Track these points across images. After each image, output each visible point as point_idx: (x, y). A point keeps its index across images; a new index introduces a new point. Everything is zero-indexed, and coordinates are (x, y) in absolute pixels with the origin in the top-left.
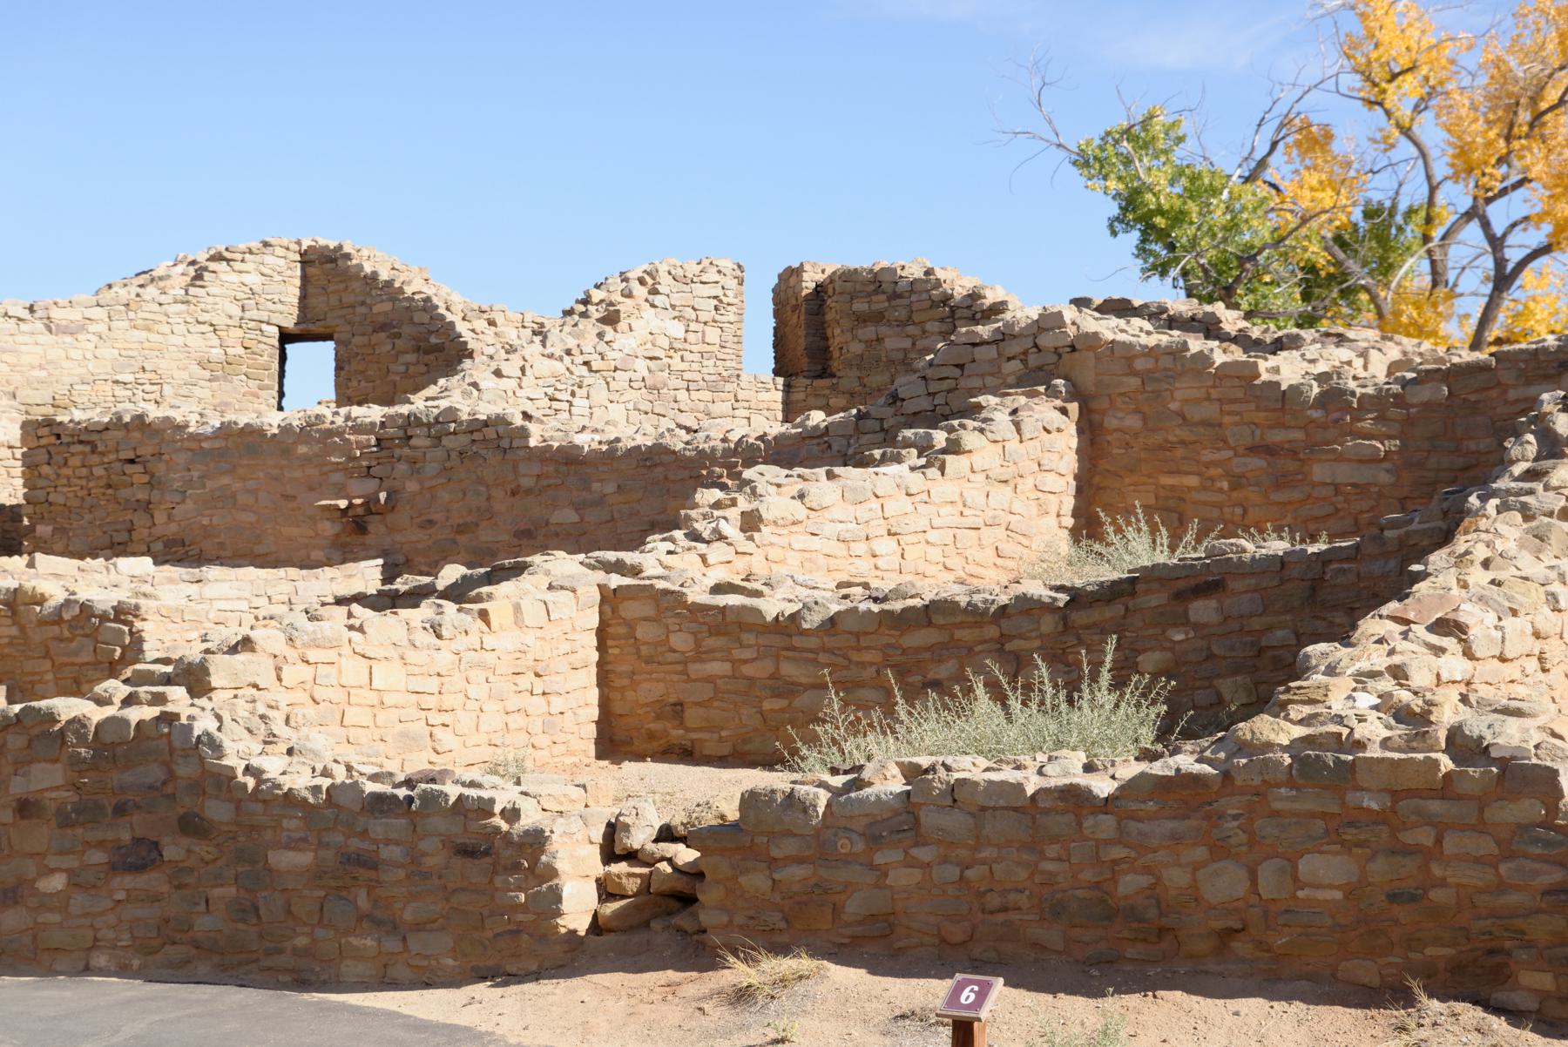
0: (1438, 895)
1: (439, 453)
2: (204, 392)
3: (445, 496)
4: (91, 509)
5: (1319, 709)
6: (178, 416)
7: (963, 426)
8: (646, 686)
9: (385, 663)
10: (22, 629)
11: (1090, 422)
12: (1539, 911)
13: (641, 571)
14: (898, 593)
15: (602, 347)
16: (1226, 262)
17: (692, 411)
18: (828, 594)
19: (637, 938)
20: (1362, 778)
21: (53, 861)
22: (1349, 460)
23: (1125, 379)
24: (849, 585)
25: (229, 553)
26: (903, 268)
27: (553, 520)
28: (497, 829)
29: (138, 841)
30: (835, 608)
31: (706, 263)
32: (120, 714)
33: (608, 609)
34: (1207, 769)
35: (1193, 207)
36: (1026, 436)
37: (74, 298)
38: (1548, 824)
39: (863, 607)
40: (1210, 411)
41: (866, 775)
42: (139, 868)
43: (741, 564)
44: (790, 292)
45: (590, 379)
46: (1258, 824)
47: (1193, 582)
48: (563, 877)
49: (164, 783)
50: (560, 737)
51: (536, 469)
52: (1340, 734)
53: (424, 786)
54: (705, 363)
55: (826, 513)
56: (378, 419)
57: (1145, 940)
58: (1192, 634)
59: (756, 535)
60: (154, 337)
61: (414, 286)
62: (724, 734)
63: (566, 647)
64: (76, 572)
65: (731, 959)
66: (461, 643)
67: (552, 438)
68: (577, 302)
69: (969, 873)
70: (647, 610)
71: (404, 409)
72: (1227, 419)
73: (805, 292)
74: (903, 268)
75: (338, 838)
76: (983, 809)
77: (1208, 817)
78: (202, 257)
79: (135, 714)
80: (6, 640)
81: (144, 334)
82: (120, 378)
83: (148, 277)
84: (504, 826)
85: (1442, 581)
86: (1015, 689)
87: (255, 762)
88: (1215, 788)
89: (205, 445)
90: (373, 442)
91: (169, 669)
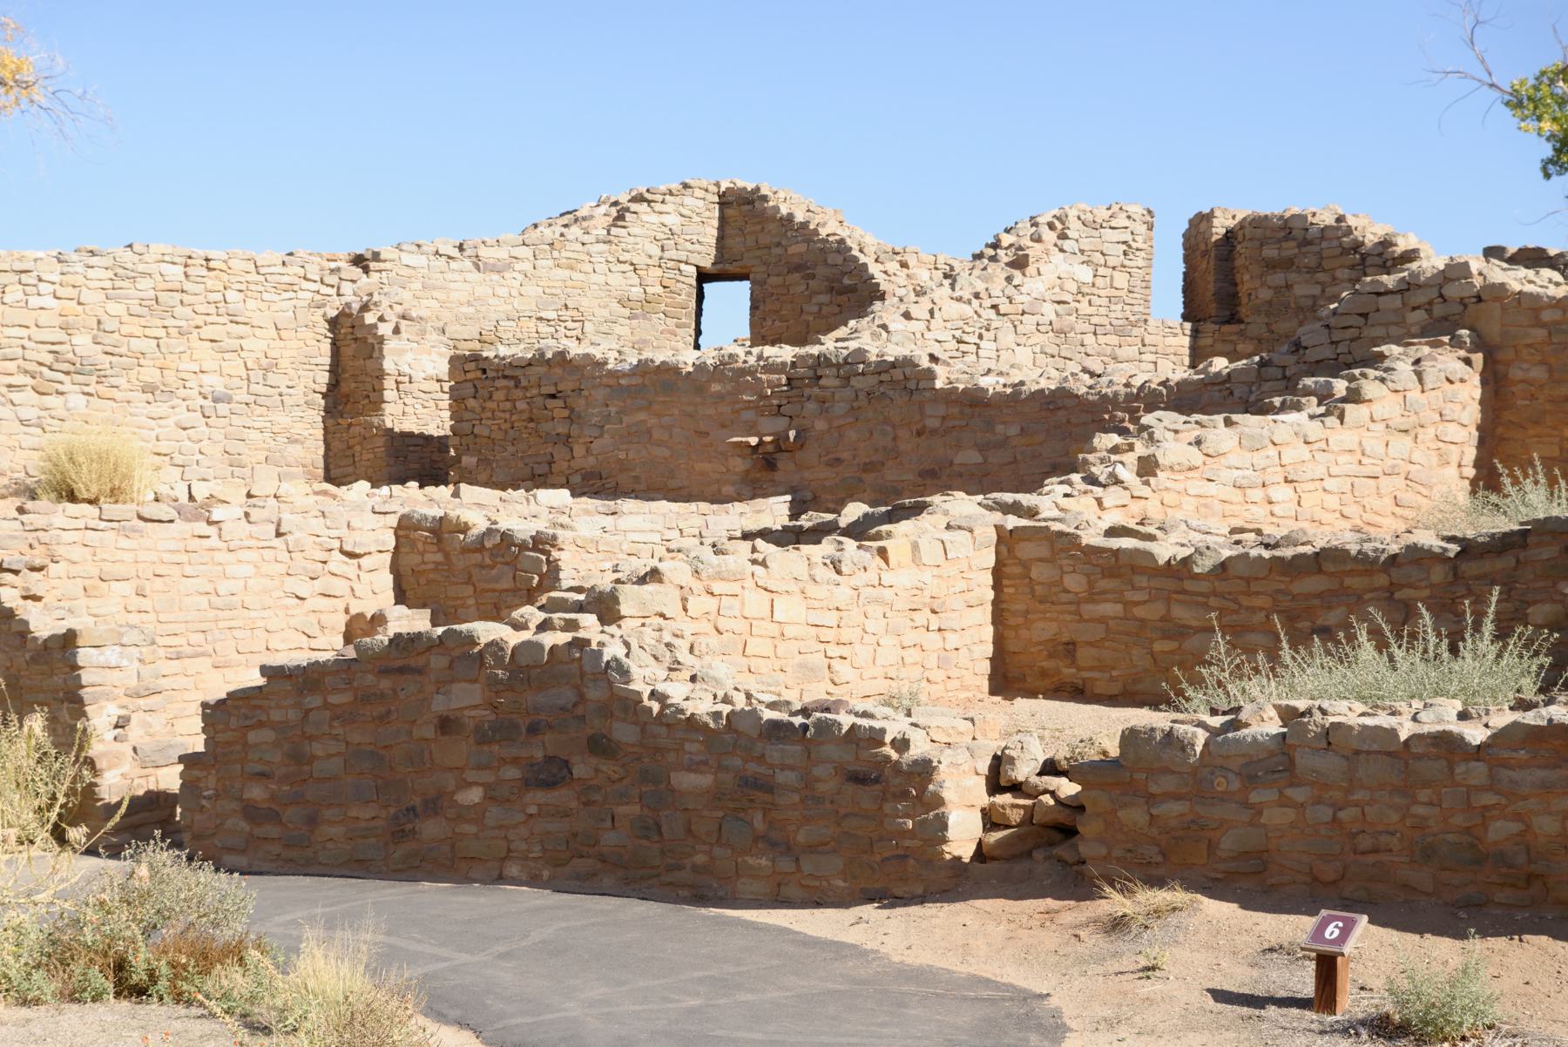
3: (852, 435)
7: (1364, 375)
8: (1040, 625)
10: (447, 555)
11: (1495, 373)
13: (1037, 513)
14: (1289, 540)
15: (1010, 291)
17: (1099, 354)
19: (1020, 867)
21: (470, 776)
24: (1242, 531)
26: (1314, 214)
27: (957, 461)
28: (887, 758)
29: (549, 759)
30: (1226, 553)
31: (1115, 208)
33: (1004, 549)
36: (1428, 385)
39: (1254, 553)
41: (1243, 716)
42: (550, 784)
43: (1136, 508)
45: (997, 322)
48: (950, 806)
49: (575, 705)
50: (954, 673)
51: (941, 410)
53: (818, 715)
54: (1113, 307)
55: (1223, 460)
56: (789, 359)
59: (1152, 480)
60: (576, 276)
61: (829, 228)
63: (962, 585)
65: (1108, 889)
66: (860, 579)
67: (957, 380)
68: (987, 246)
69: (1342, 815)
70: (1043, 551)
71: (814, 350)
73: (1214, 238)
74: (1314, 214)
75: (738, 762)
76: (1357, 753)
78: (624, 199)
79: (550, 639)
80: (432, 566)
81: (567, 273)
82: (543, 314)
83: (572, 217)
84: (894, 756)
87: (661, 687)
89: (623, 382)
90: (784, 381)
91: (582, 597)
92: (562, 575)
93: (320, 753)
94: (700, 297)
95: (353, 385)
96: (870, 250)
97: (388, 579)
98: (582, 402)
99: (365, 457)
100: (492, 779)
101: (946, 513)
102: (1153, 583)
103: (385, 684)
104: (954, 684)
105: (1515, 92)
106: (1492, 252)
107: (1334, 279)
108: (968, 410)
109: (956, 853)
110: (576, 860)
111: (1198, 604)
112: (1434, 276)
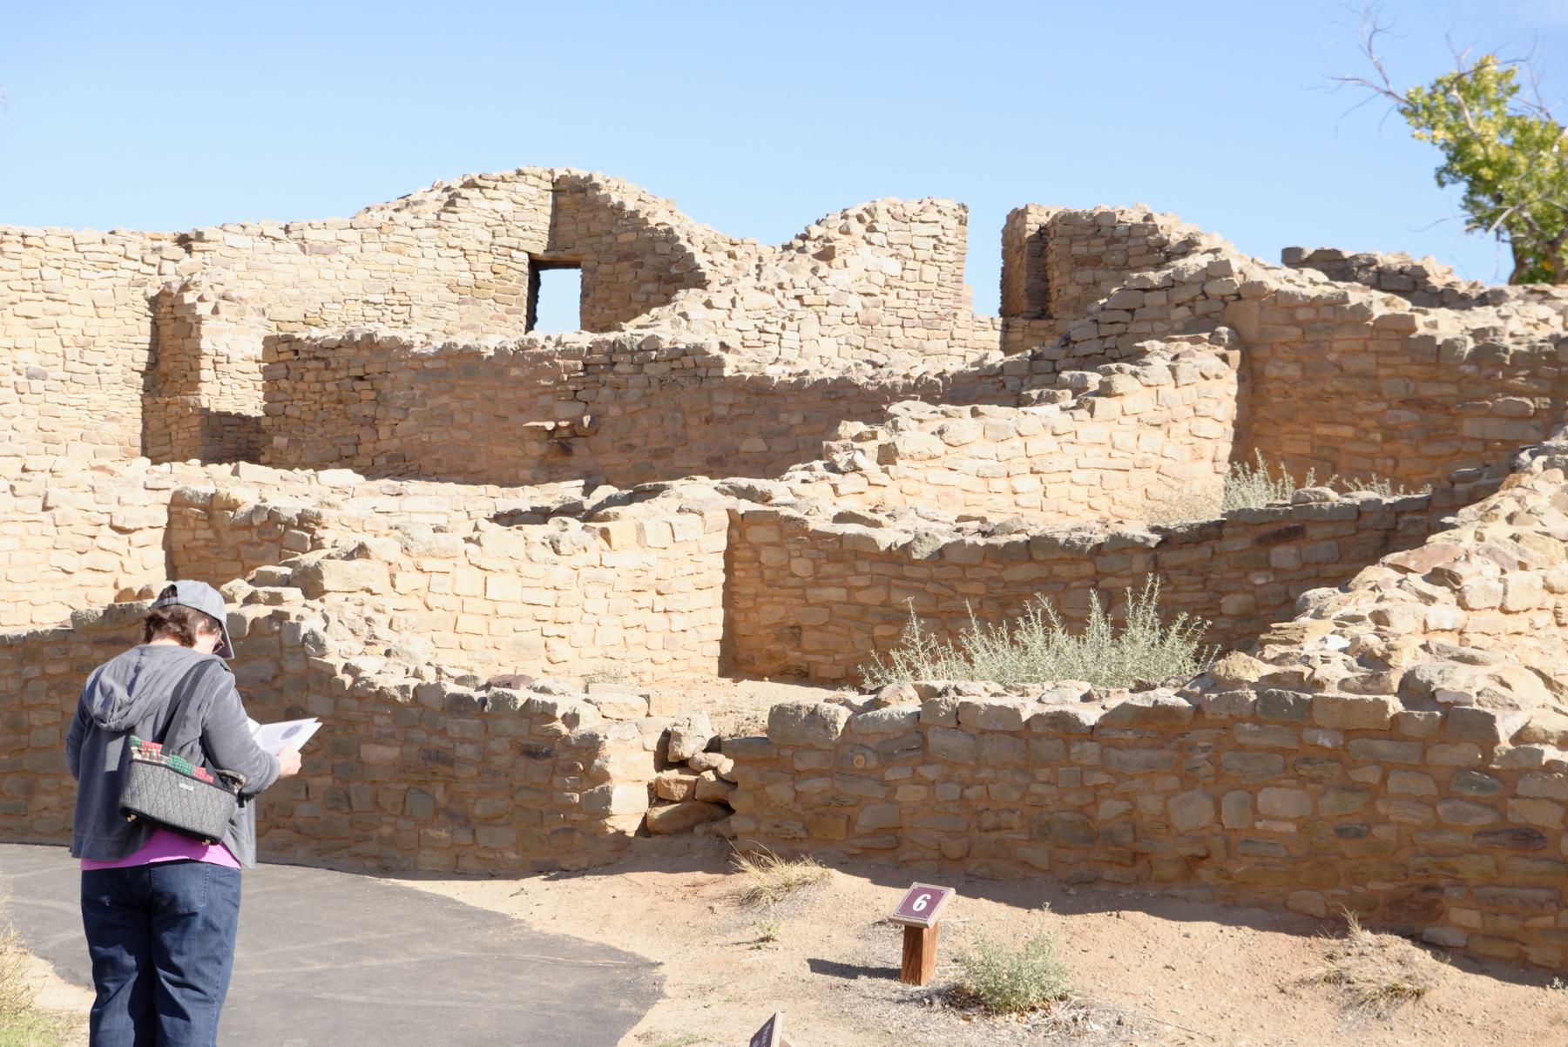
0: (1380, 832)
1: (641, 379)
2: (451, 314)
3: (644, 421)
5: (1294, 649)
7: (1120, 370)
8: (768, 608)
10: (217, 532)
11: (1252, 370)
12: (1473, 852)
14: (1004, 529)
15: (815, 282)
16: (1552, 217)
17: (906, 347)
18: (944, 527)
19: (680, 842)
20: (1318, 716)
22: (1499, 416)
23: (1287, 329)
24: (968, 519)
25: (444, 470)
26: (1122, 212)
27: (743, 448)
28: (558, 732)
30: (945, 540)
31: (927, 202)
33: (735, 533)
34: (1183, 702)
35: (1521, 160)
36: (1182, 381)
38: (1483, 768)
39: (969, 540)
40: (1365, 363)
41: (883, 696)
43: (873, 495)
45: (800, 312)
46: (1225, 756)
47: (1275, 528)
48: (614, 781)
49: (274, 677)
50: (680, 654)
51: (729, 398)
52: (1302, 674)
53: (496, 689)
54: (921, 301)
55: (965, 450)
57: (1119, 863)
58: (1272, 578)
59: (891, 468)
60: (404, 260)
61: (658, 217)
62: (838, 657)
63: (692, 568)
64: (278, 481)
65: (745, 863)
66: (580, 559)
67: (746, 369)
69: (968, 792)
70: (771, 535)
71: (611, 336)
72: (1383, 372)
74: (1122, 212)
75: (423, 735)
76: (983, 732)
77: (1180, 748)
78: (456, 184)
81: (395, 257)
83: (408, 203)
84: (564, 730)
85: (1464, 537)
86: (1035, 614)
87: (354, 661)
88: (1187, 721)
89: (427, 365)
90: (580, 367)
93: (37, 723)
94: (534, 284)
95: (172, 365)
96: (697, 240)
97: (161, 555)
98: (388, 384)
99: (182, 436)
101: (680, 496)
104: (676, 666)
105: (1410, 101)
106: (1292, 257)
108: (754, 399)
109: (620, 828)
110: (273, 831)
112: (1197, 273)
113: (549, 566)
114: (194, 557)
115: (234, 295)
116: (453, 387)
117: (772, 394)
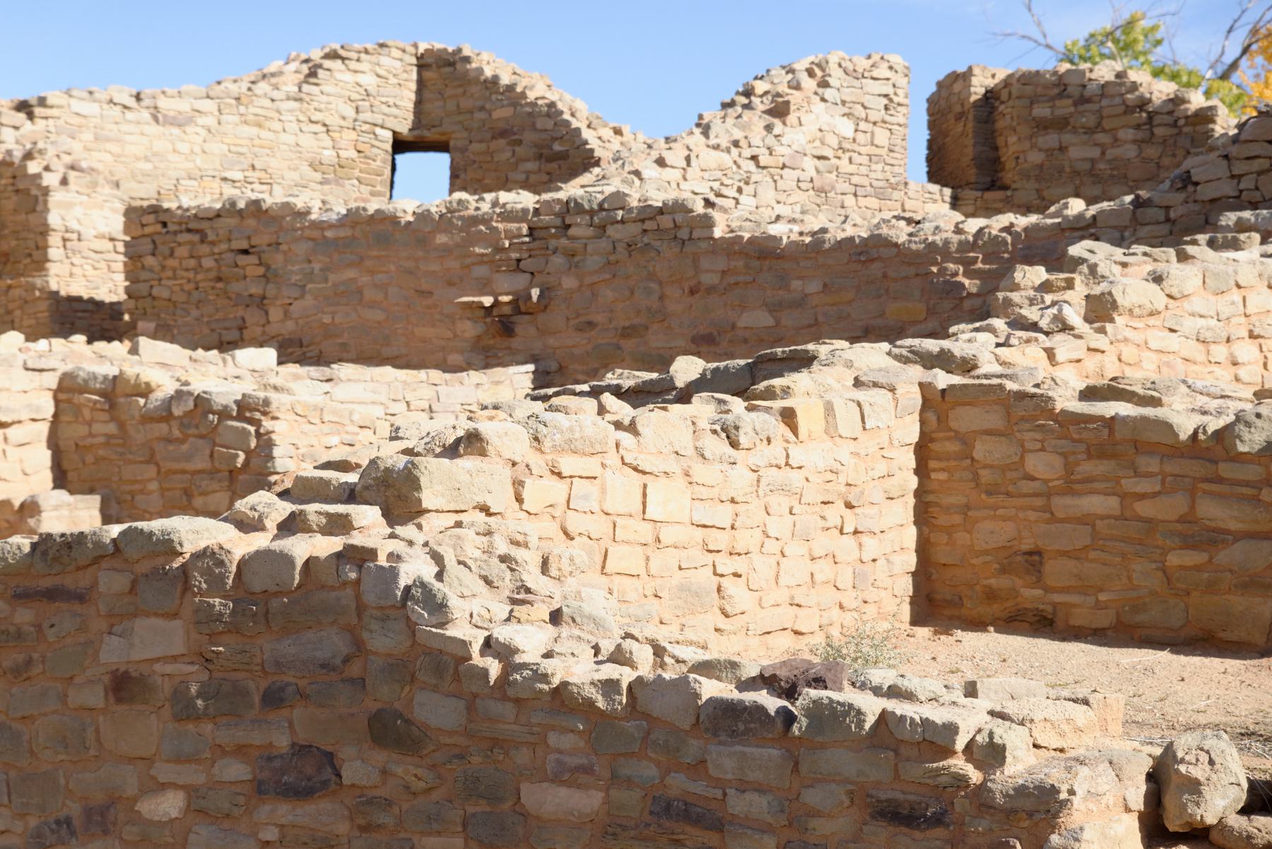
1: (604, 244)
3: (607, 294)
4: (198, 304)
6: (299, 203)
8: (987, 525)
9: (663, 480)
10: (122, 426)
13: (975, 367)
15: (770, 140)
21: (164, 772)
28: (961, 780)
29: (301, 750)
31: (876, 57)
32: (278, 545)
33: (931, 416)
37: (184, 88)
42: (300, 793)
44: (954, 99)
49: (346, 660)
50: (871, 595)
51: (721, 263)
53: (814, 693)
54: (874, 167)
55: (1185, 304)
56: (531, 206)
59: (1109, 327)
60: (265, 134)
61: (538, 90)
62: (1103, 597)
63: (882, 468)
64: (186, 362)
66: (763, 455)
67: (740, 228)
68: (738, 93)
70: (994, 420)
73: (973, 98)
75: (649, 771)
78: (316, 55)
79: (303, 548)
80: (102, 439)
81: (254, 131)
82: (228, 175)
84: (975, 776)
87: (503, 634)
89: (329, 234)
90: (525, 231)
91: (352, 478)
92: (276, 452)
95: (14, 243)
97: (45, 456)
98: (280, 257)
100: (201, 779)
101: (849, 364)
102: (1168, 468)
103: (24, 616)
104: (871, 610)
107: (1116, 140)
108: (756, 263)
111: (1242, 498)
113: (726, 467)
114: (89, 458)
115: (84, 165)
116: (362, 259)
117: (780, 257)
